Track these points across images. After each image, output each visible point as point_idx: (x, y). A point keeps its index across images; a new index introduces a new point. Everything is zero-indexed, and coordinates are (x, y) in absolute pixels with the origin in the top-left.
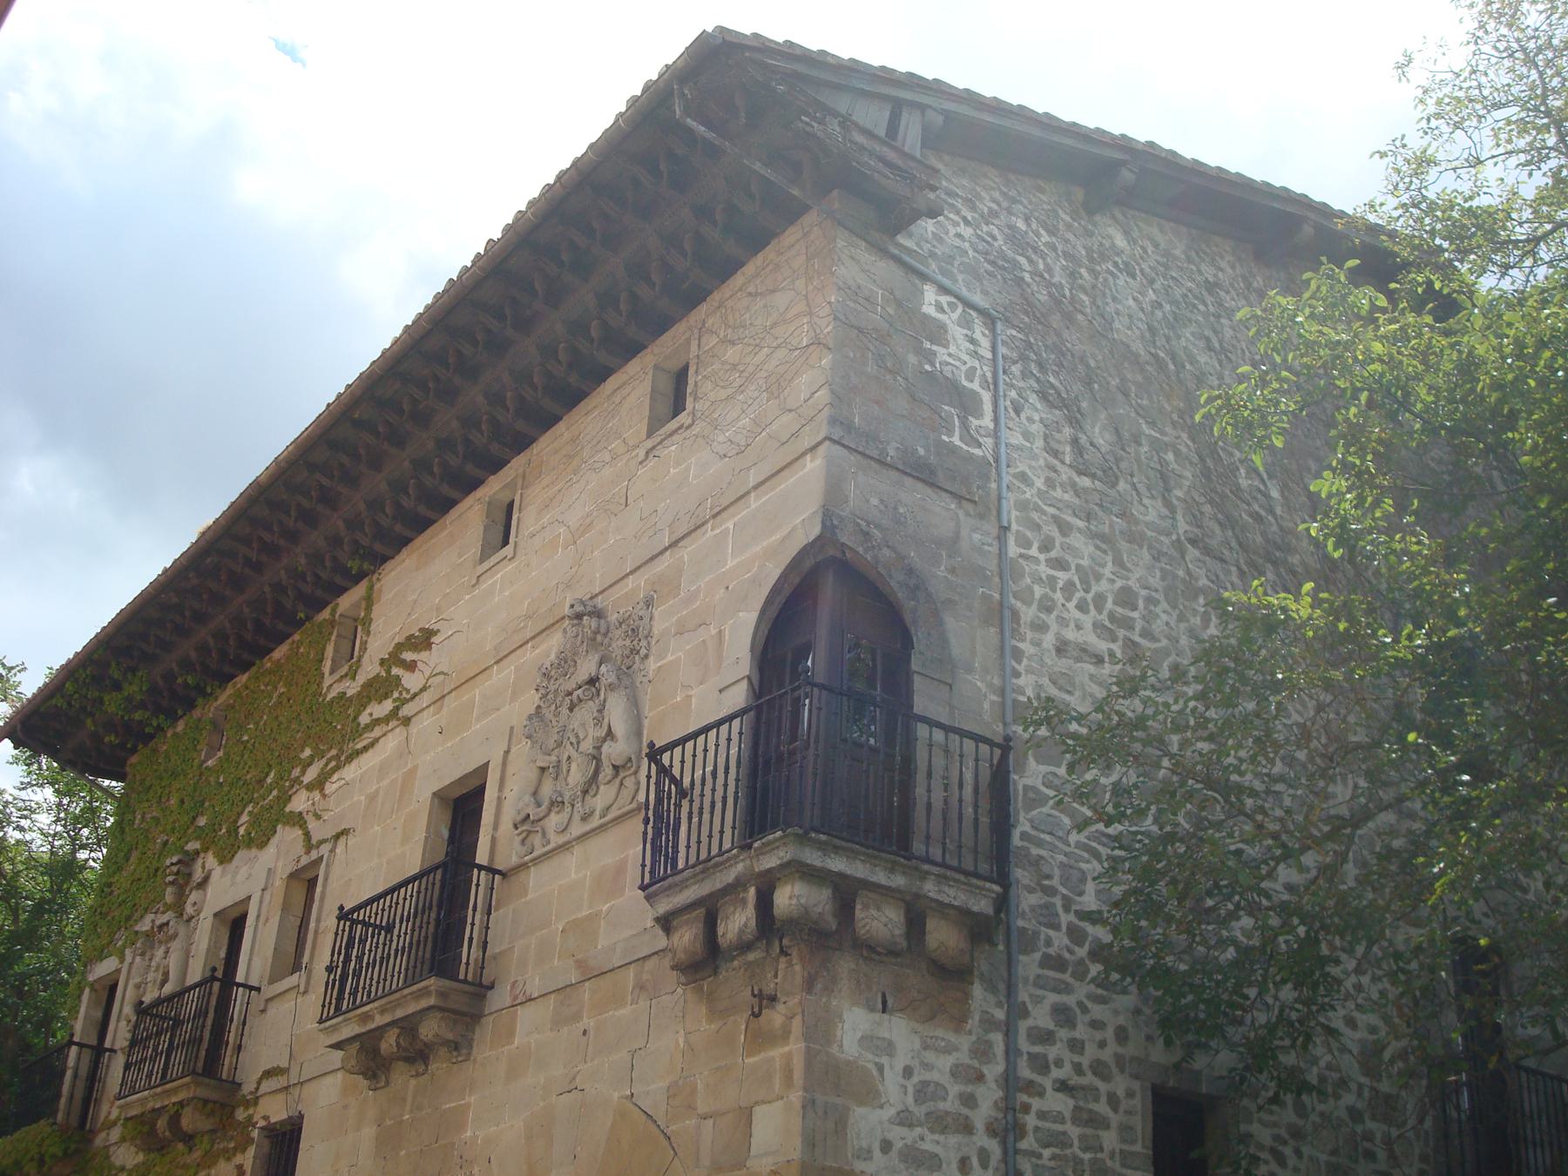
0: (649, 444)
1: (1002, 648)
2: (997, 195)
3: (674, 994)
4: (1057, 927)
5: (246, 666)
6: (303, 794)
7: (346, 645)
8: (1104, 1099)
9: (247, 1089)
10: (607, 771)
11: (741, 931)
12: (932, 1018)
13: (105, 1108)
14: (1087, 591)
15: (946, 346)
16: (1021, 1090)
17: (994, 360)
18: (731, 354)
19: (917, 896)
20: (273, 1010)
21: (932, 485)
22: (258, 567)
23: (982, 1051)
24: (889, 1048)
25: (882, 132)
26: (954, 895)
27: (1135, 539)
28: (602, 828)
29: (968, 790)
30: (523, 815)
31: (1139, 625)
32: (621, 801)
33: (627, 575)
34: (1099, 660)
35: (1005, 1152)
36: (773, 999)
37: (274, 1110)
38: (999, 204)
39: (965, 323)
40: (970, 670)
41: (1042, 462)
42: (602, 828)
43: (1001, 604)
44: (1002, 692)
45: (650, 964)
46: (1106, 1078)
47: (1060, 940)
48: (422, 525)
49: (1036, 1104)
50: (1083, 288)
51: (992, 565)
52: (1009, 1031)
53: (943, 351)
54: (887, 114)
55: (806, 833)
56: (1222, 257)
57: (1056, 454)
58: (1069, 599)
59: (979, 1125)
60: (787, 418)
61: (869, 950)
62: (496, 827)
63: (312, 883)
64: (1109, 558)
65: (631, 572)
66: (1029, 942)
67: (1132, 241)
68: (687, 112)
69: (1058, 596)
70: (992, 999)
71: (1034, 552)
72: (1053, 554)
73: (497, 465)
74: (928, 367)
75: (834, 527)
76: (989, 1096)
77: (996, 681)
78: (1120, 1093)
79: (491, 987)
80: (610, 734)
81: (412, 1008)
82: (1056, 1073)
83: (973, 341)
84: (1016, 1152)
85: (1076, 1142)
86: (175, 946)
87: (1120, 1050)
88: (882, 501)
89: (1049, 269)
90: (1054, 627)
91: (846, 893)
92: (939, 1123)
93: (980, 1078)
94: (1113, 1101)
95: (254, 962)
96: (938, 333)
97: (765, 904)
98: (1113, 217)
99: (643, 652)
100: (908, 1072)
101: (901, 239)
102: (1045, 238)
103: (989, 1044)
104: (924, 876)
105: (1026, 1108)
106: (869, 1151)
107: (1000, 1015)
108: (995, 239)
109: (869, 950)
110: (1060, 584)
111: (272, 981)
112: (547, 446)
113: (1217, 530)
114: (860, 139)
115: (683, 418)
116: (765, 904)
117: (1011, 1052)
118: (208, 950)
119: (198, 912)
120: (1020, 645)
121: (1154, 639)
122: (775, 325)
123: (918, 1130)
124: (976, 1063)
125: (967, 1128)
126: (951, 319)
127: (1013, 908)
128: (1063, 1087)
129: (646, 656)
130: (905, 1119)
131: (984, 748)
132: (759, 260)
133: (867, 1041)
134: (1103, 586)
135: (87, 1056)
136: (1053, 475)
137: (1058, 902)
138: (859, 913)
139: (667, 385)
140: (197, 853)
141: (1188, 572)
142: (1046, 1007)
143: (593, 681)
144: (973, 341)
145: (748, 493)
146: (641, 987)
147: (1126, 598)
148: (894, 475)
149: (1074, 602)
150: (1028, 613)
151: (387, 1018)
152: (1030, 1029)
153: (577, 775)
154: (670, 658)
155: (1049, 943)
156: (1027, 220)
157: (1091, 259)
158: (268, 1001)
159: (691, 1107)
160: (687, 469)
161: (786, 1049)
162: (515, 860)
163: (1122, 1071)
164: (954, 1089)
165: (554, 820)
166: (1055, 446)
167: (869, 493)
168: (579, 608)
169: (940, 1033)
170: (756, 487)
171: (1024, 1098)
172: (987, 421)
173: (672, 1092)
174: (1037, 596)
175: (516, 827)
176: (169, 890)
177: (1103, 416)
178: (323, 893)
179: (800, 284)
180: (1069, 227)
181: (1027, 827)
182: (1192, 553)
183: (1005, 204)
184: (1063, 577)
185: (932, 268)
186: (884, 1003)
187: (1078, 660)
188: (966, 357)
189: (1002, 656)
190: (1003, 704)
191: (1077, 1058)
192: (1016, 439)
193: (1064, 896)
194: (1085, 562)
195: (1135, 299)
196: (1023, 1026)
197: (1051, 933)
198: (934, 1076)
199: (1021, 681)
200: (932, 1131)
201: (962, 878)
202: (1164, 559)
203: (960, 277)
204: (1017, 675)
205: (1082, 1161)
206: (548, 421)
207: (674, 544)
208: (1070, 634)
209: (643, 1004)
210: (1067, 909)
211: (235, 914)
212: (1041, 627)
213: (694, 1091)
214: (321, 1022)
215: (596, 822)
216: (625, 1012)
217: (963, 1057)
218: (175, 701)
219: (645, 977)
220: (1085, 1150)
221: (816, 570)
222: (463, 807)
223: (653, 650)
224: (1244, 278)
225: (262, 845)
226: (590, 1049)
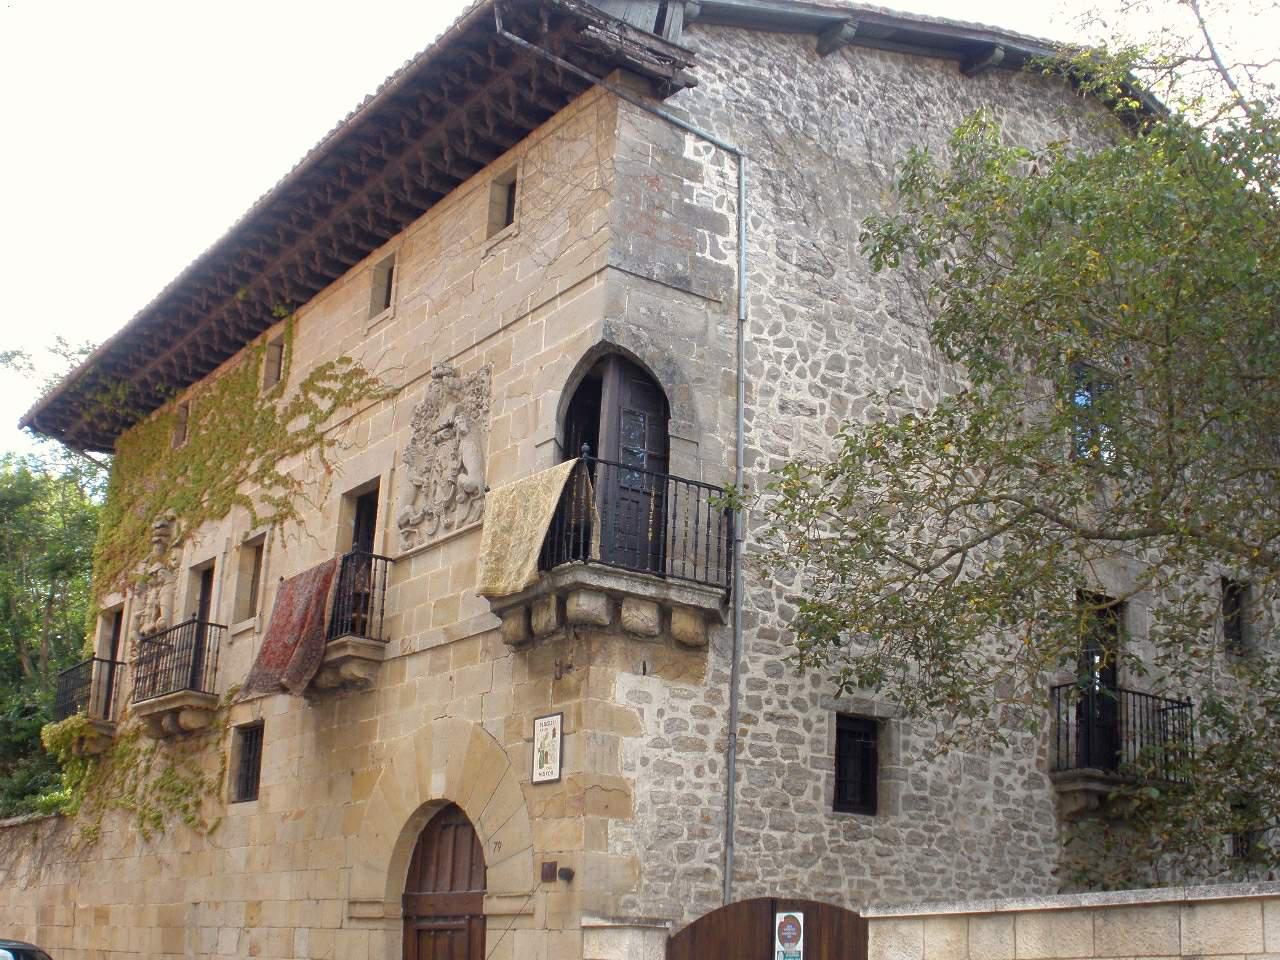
0: (488, 245)
1: (738, 411)
2: (747, 51)
3: (507, 658)
4: (769, 609)
5: (201, 376)
6: (248, 484)
7: (274, 367)
8: (801, 724)
9: (222, 700)
10: (460, 496)
11: (547, 625)
13: (121, 704)
14: (805, 361)
15: (702, 182)
16: (742, 720)
17: (739, 188)
18: (545, 183)
19: (665, 600)
20: (238, 644)
21: (689, 293)
22: (208, 310)
23: (714, 696)
24: (647, 698)
25: (651, 28)
26: (689, 598)
27: (843, 317)
28: (459, 536)
29: (703, 526)
31: (844, 384)
32: (471, 518)
34: (813, 412)
35: (728, 762)
38: (748, 58)
39: (717, 161)
40: (713, 430)
41: (774, 265)
42: (459, 536)
43: (738, 377)
44: (737, 444)
46: (803, 709)
47: (773, 617)
49: (751, 728)
50: (814, 119)
51: (732, 348)
52: (733, 682)
53: (698, 185)
54: (656, 12)
56: (932, 75)
57: (785, 257)
58: (790, 369)
59: (711, 746)
60: (582, 243)
61: (632, 635)
62: (387, 524)
63: (259, 549)
64: (824, 334)
66: (750, 620)
67: (856, 72)
68: (506, 27)
69: (783, 368)
70: (721, 660)
71: (765, 335)
72: (780, 335)
73: (381, 242)
74: (687, 200)
75: (612, 333)
76: (718, 725)
77: (733, 436)
78: (813, 719)
80: (462, 469)
82: (767, 708)
83: (722, 175)
84: (736, 761)
86: (164, 590)
87: (814, 690)
88: (649, 310)
89: (787, 108)
90: (778, 390)
91: (616, 600)
92: (683, 745)
93: (712, 714)
94: (808, 725)
95: (222, 607)
96: (694, 172)
98: (843, 55)
99: (485, 408)
100: (661, 713)
101: (669, 101)
102: (785, 80)
103: (719, 691)
104: (669, 586)
105: (744, 733)
106: (634, 765)
107: (727, 671)
108: (744, 88)
109: (632, 635)
110: (785, 358)
111: (237, 621)
113: (913, 302)
114: (632, 36)
115: (511, 229)
117: (734, 696)
119: (178, 565)
120: (752, 407)
121: (857, 392)
122: (575, 167)
123: (667, 750)
124: (709, 705)
125: (702, 747)
126: (705, 160)
127: (739, 597)
128: (771, 717)
130: (657, 743)
131: (715, 493)
133: (633, 694)
134: (819, 355)
135: (106, 667)
136: (782, 273)
137: (773, 591)
138: (625, 613)
139: (501, 194)
140: (173, 519)
141: (887, 338)
142: (761, 664)
143: (450, 426)
144: (722, 175)
146: (486, 651)
147: (836, 363)
148: (659, 286)
149: (795, 370)
150: (758, 383)
152: (748, 680)
153: (441, 497)
154: (503, 415)
155: (764, 620)
156: (771, 68)
157: (822, 93)
158: (235, 636)
159: (519, 734)
160: (515, 270)
162: (400, 553)
163: (815, 704)
164: (693, 722)
166: (786, 251)
167: (638, 303)
168: (439, 370)
169: (683, 686)
170: (561, 294)
171: (744, 726)
172: (732, 238)
173: (508, 723)
174: (766, 368)
175: (400, 527)
176: (156, 547)
177: (824, 222)
178: (268, 561)
179: (593, 137)
180: (805, 69)
181: (752, 541)
182: (892, 321)
183: (753, 57)
184: (786, 352)
185: (693, 121)
187: (797, 413)
188: (716, 189)
189: (737, 417)
190: (737, 453)
191: (782, 698)
192: (755, 248)
193: (778, 587)
194: (804, 340)
195: (856, 121)
196: (743, 678)
197: (767, 613)
198: (679, 715)
199: (751, 434)
201: (696, 586)
202: (867, 330)
203: (714, 125)
204: (748, 429)
205: (783, 766)
207: (505, 328)
208: (791, 396)
210: (779, 595)
211: (205, 568)
212: (769, 392)
213: (521, 724)
215: (454, 531)
217: (700, 701)
218: (148, 401)
220: (785, 758)
221: (601, 360)
222: (364, 503)
223: (492, 407)
224: (950, 90)
225: (222, 515)
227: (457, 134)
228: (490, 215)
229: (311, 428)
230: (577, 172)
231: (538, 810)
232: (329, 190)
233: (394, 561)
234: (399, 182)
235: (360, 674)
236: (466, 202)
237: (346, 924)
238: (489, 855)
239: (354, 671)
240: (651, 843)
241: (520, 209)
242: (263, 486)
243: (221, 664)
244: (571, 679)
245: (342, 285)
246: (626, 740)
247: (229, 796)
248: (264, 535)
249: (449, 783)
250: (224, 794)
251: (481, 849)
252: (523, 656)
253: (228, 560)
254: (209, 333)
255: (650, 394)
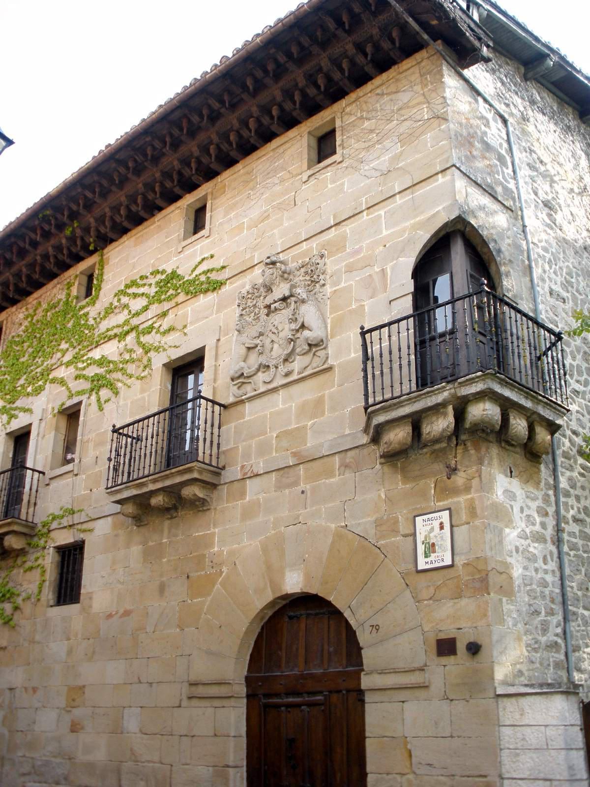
0: (310, 172)
11: (444, 430)
12: (528, 482)
20: (54, 484)
30: (239, 373)
33: (302, 242)
36: (455, 469)
37: (65, 538)
45: (350, 454)
48: (138, 221)
55: (496, 374)
65: (305, 240)
79: (224, 468)
81: (178, 479)
85: (581, 549)
97: (460, 415)
99: (322, 282)
103: (548, 495)
111: (52, 469)
112: (227, 177)
116: (460, 415)
118: (503, 396)
122: (400, 109)
129: (324, 285)
132: (385, 76)
145: (394, 195)
151: (159, 485)
158: (51, 479)
161: (469, 496)
162: (231, 400)
165: (261, 376)
173: (378, 523)
175: (233, 380)
186: (511, 472)
200: (533, 542)
206: (230, 163)
209: (348, 475)
214: (107, 488)
216: (335, 480)
219: (348, 461)
226: (309, 501)
227: (116, 209)
228: (309, 154)
229: (127, 322)
230: (402, 112)
231: (425, 594)
232: (168, 139)
233: (224, 407)
234: (87, 230)
235: (201, 495)
236: (281, 150)
237: (185, 703)
238: (363, 638)
239: (197, 491)
240: (527, 619)
241: (342, 145)
242: (77, 368)
243: (38, 502)
244: (459, 479)
245: (155, 223)
246: (507, 530)
247: (48, 601)
248: (80, 403)
249: (308, 577)
250: (43, 598)
251: (355, 632)
252: (394, 466)
253: (43, 424)
254: (18, 275)
255: (483, 262)
